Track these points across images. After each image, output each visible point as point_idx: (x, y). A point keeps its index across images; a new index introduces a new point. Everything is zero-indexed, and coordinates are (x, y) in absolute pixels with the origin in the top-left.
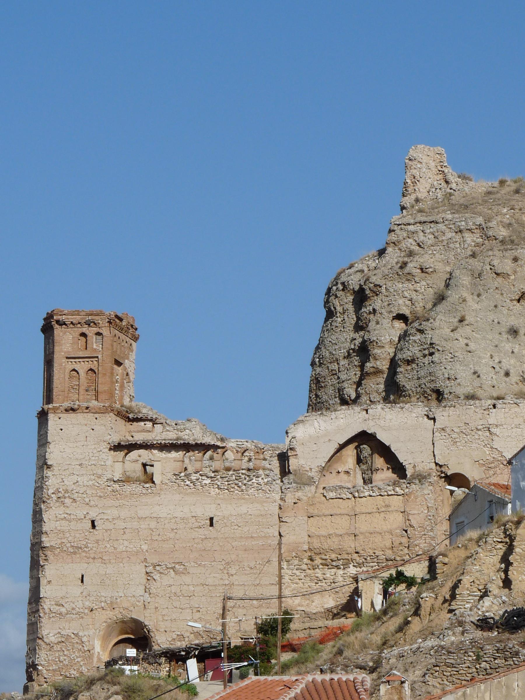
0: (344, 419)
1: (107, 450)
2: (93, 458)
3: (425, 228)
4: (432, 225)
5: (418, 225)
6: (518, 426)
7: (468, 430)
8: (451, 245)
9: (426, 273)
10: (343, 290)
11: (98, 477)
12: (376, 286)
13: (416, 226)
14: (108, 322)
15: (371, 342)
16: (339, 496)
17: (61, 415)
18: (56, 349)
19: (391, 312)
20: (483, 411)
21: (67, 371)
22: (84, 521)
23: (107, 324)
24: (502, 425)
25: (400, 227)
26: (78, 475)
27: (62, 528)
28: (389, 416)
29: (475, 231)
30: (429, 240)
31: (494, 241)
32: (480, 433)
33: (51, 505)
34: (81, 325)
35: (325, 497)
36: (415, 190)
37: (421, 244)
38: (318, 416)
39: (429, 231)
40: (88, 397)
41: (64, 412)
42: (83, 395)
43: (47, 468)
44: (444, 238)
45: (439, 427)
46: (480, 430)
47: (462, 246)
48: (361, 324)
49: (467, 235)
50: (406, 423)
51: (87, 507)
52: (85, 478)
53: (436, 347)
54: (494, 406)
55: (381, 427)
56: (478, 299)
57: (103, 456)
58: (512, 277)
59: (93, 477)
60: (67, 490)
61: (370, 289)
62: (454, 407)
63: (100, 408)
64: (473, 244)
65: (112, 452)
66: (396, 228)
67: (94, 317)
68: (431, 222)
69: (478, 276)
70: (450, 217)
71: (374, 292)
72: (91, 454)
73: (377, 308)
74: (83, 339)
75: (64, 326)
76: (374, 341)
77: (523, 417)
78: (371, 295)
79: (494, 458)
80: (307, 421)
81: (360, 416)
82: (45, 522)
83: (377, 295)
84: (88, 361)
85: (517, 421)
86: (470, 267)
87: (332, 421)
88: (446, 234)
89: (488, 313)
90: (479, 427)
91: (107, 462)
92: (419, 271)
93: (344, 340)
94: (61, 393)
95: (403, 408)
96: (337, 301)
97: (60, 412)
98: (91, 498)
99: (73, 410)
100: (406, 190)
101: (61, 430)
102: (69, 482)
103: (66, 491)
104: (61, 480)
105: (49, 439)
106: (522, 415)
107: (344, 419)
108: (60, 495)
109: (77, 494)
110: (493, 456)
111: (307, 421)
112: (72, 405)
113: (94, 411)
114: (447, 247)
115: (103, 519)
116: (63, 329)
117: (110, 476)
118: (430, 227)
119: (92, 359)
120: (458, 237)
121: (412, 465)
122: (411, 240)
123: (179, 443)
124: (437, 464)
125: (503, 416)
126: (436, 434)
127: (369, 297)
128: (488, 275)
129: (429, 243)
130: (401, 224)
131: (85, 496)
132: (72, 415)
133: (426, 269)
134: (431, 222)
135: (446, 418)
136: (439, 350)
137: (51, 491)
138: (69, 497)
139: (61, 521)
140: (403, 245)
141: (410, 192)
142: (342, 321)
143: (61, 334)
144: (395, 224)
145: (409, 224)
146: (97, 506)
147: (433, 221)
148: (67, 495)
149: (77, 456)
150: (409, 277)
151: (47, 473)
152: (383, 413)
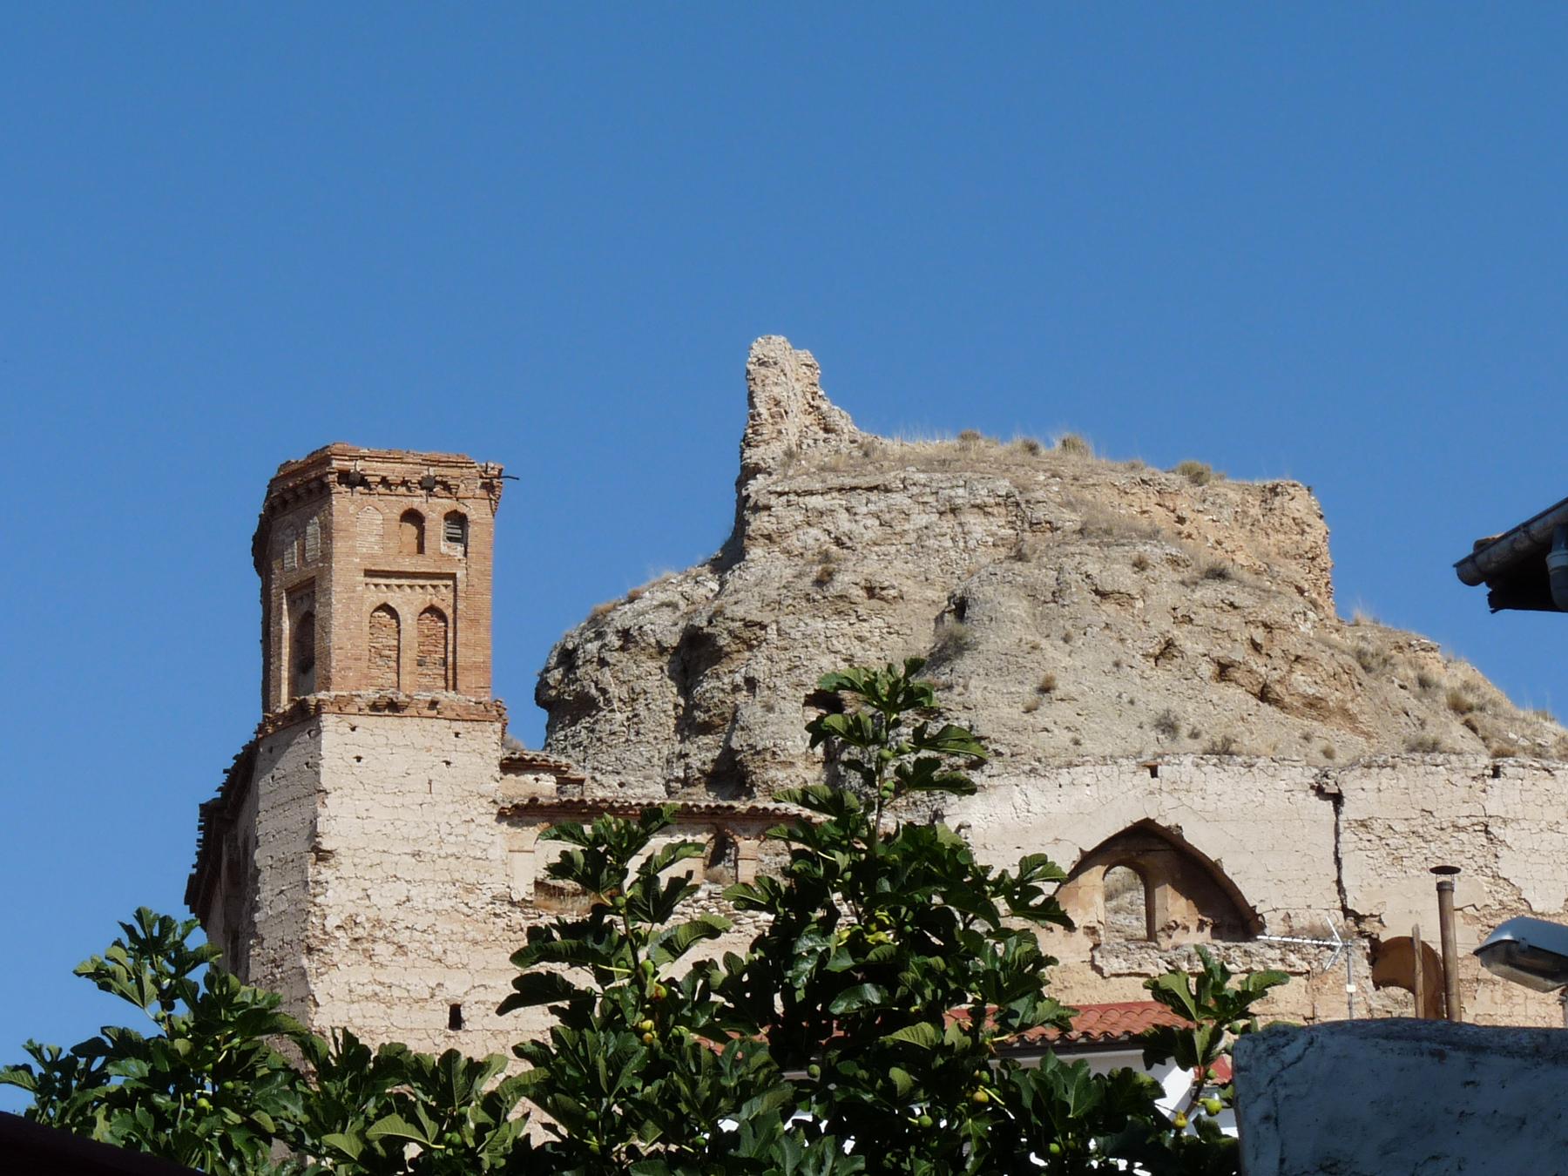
0: (1094, 788)
1: (491, 819)
2: (452, 839)
3: (854, 502)
4: (873, 496)
5: (835, 494)
6: (1554, 827)
7: (1431, 827)
8: (931, 542)
9: (882, 599)
10: (622, 649)
11: (467, 891)
12: (748, 624)
13: (828, 497)
14: (484, 486)
15: (758, 753)
16: (1137, 970)
17: (356, 720)
18: (339, 546)
19: (801, 685)
20: (1469, 782)
21: (367, 608)
22: (430, 1005)
23: (483, 493)
24: (1517, 820)
25: (784, 498)
26: (408, 882)
27: (368, 1022)
28: (1213, 786)
29: (995, 510)
30: (868, 529)
31: (1049, 534)
32: (1462, 836)
33: (336, 959)
34: (409, 489)
35: (1099, 970)
36: (780, 432)
37: (845, 539)
38: (1023, 777)
39: (864, 510)
40: (425, 681)
41: (367, 711)
42: (411, 673)
43: (319, 859)
44: (907, 527)
45: (1352, 817)
46: (1464, 829)
47: (961, 544)
48: (700, 716)
49: (973, 520)
50: (1262, 804)
51: (438, 968)
52: (431, 892)
53: (991, 747)
54: (1496, 773)
55: (1195, 812)
56: (1068, 648)
57: (479, 834)
58: (1139, 604)
59: (452, 890)
60: (379, 921)
61: (730, 632)
62: (1394, 767)
63: (467, 708)
64: (990, 540)
65: (505, 825)
66: (773, 500)
67: (445, 471)
68: (870, 489)
69: (1050, 597)
70: (922, 477)
71: (744, 642)
72: (445, 829)
73: (760, 676)
74: (411, 530)
75: (360, 488)
76: (766, 749)
77: (1564, 804)
78: (734, 647)
79: (1501, 903)
80: (995, 787)
81: (1136, 780)
82: (317, 1005)
83: (750, 648)
84: (422, 587)
85: (1552, 814)
86: (1020, 579)
87: (1061, 791)
88: (913, 517)
89: (1103, 678)
90: (1463, 822)
91: (491, 850)
92: (862, 593)
93: (642, 762)
94: (351, 663)
95: (1251, 766)
96: (608, 674)
97: (355, 710)
98: (449, 946)
99: (394, 707)
100: (755, 433)
101: (359, 759)
102: (385, 900)
103: (378, 923)
104: (361, 894)
105: (326, 781)
106: (1562, 799)
107: (1094, 788)
108: (359, 932)
109: (408, 932)
110: (1500, 897)
111: (995, 787)
112: (389, 693)
113: (453, 715)
114: (919, 547)
115: (484, 1003)
116: (357, 496)
117: (500, 889)
118: (868, 501)
119: (435, 582)
120: (947, 524)
121: (1281, 914)
122: (814, 532)
123: (703, 805)
124: (1347, 912)
125: (1517, 799)
126: (1346, 836)
127: (727, 654)
128: (1080, 596)
129: (866, 537)
130: (787, 493)
131: (432, 938)
132: (389, 722)
133: (883, 589)
134: (870, 489)
135: (1372, 796)
136: (998, 754)
137: (331, 923)
138: (385, 938)
139: (364, 1003)
140: (794, 542)
141: (766, 437)
142: (628, 719)
143: (352, 509)
144: (770, 493)
145: (812, 493)
146: (464, 966)
147: (876, 487)
148: (379, 934)
149: (405, 830)
150: (842, 605)
151: (320, 873)
152: (1198, 777)
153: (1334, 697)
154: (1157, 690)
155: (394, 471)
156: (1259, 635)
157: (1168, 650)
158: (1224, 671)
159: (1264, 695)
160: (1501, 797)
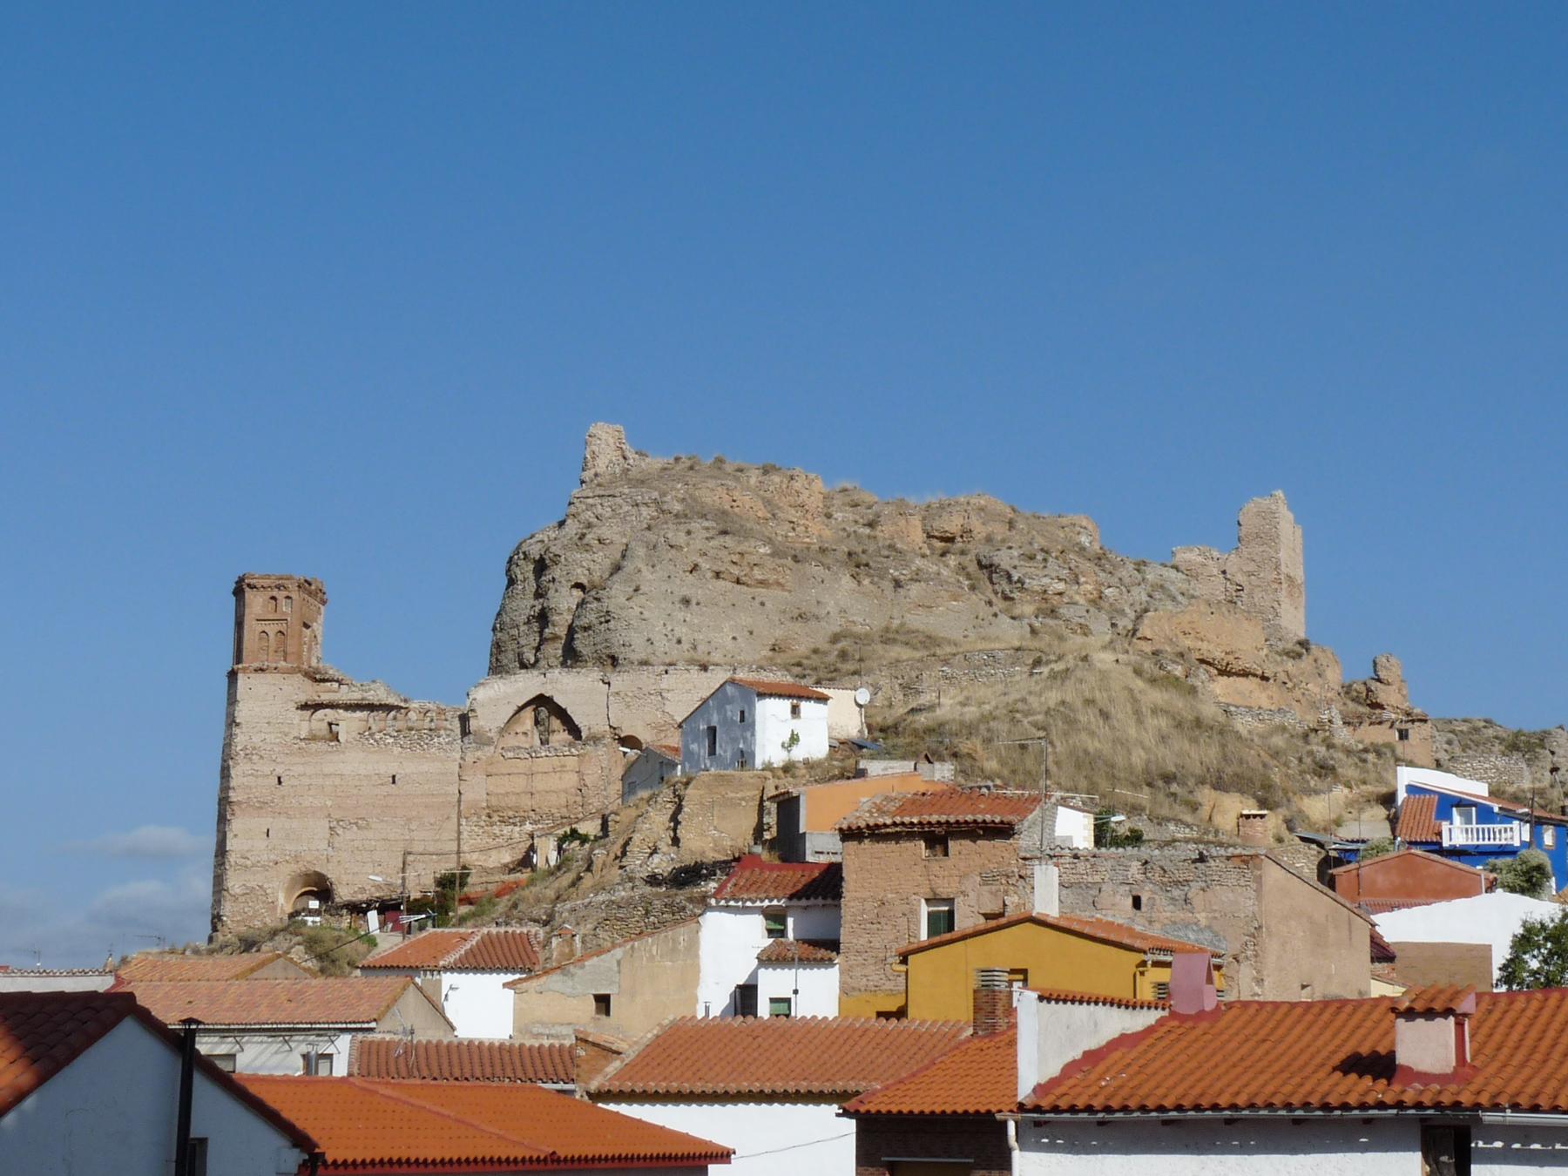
30: (607, 512)
49: (643, 509)
102: (256, 739)
120: (634, 511)
128: (663, 547)
132: (261, 675)
150: (588, 548)
153: (772, 577)
154: (687, 585)
155: (266, 582)
156: (735, 558)
157: (695, 568)
158: (718, 575)
159: (738, 582)
160: (666, 682)
